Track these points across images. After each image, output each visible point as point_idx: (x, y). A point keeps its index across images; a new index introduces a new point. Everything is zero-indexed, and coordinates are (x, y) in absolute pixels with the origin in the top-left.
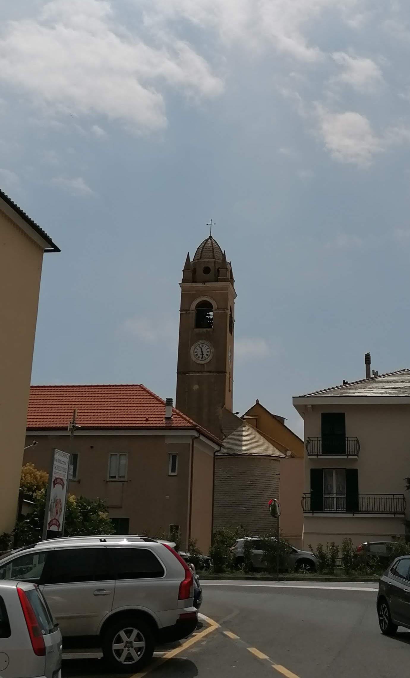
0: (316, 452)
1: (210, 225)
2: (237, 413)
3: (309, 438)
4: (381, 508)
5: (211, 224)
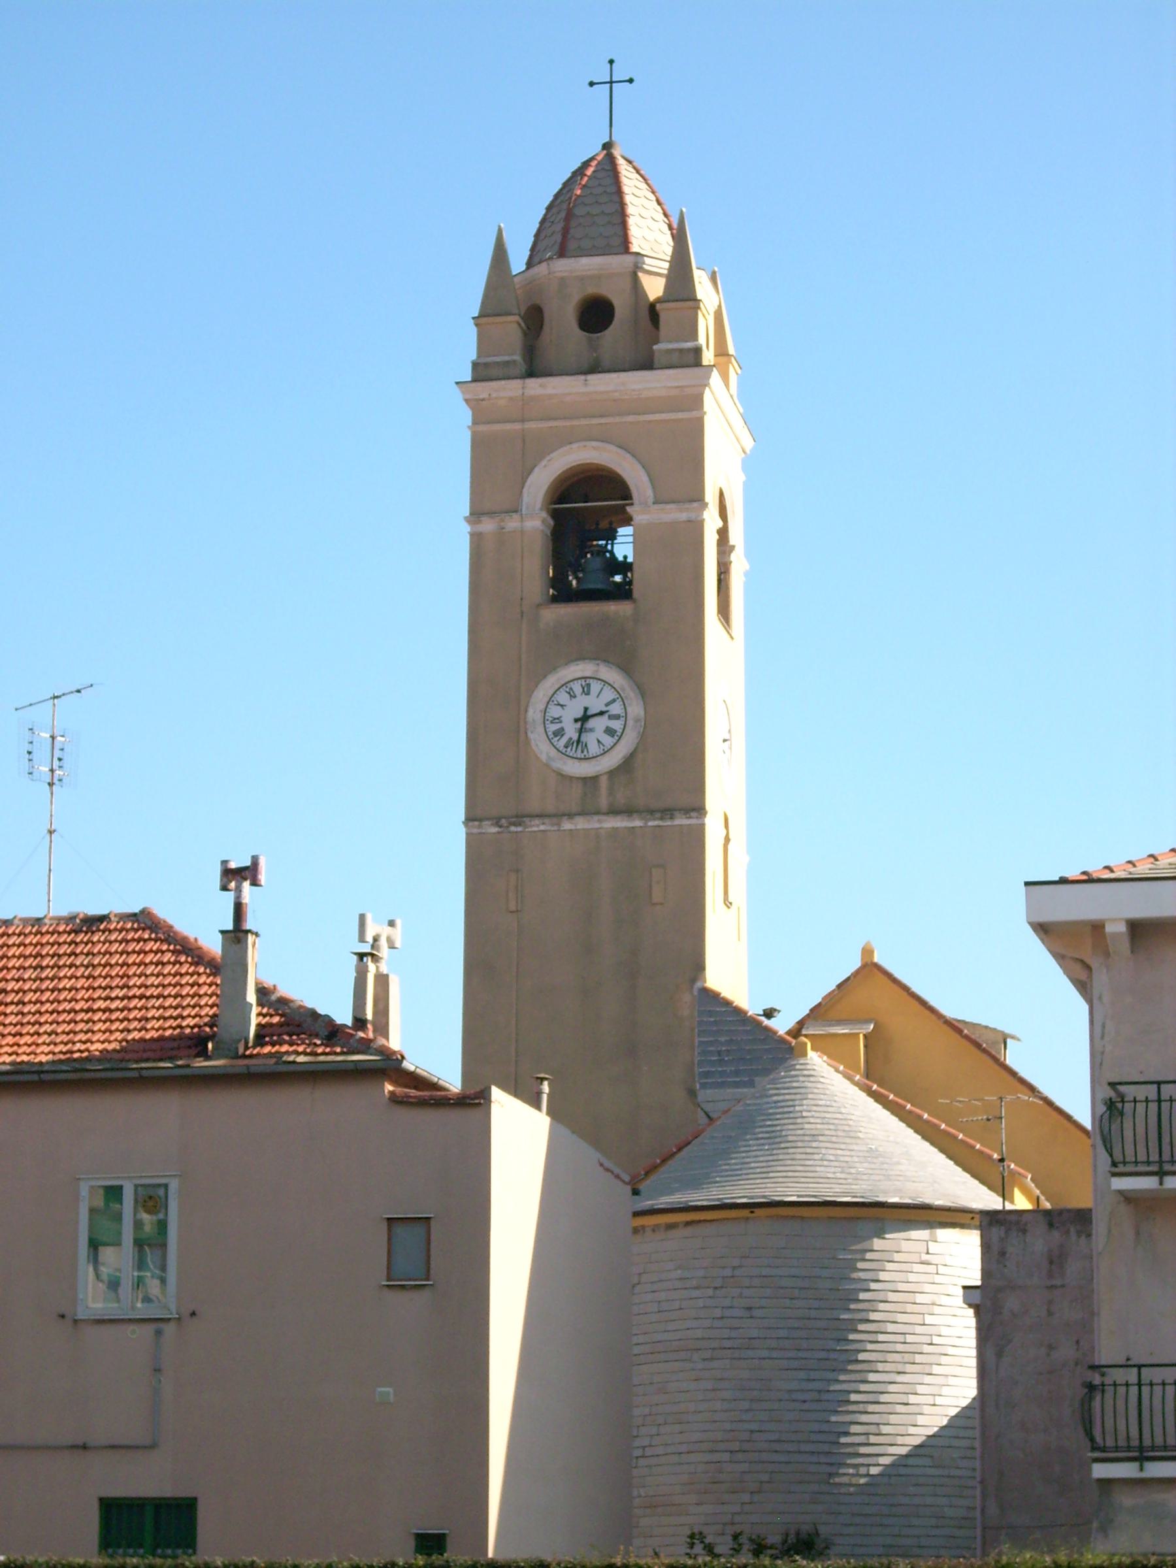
0: (1154, 1157)
1: (608, 85)
2: (769, 1014)
3: (1116, 1091)
4: (1158, 1431)
5: (611, 82)
